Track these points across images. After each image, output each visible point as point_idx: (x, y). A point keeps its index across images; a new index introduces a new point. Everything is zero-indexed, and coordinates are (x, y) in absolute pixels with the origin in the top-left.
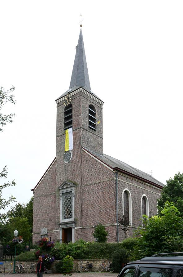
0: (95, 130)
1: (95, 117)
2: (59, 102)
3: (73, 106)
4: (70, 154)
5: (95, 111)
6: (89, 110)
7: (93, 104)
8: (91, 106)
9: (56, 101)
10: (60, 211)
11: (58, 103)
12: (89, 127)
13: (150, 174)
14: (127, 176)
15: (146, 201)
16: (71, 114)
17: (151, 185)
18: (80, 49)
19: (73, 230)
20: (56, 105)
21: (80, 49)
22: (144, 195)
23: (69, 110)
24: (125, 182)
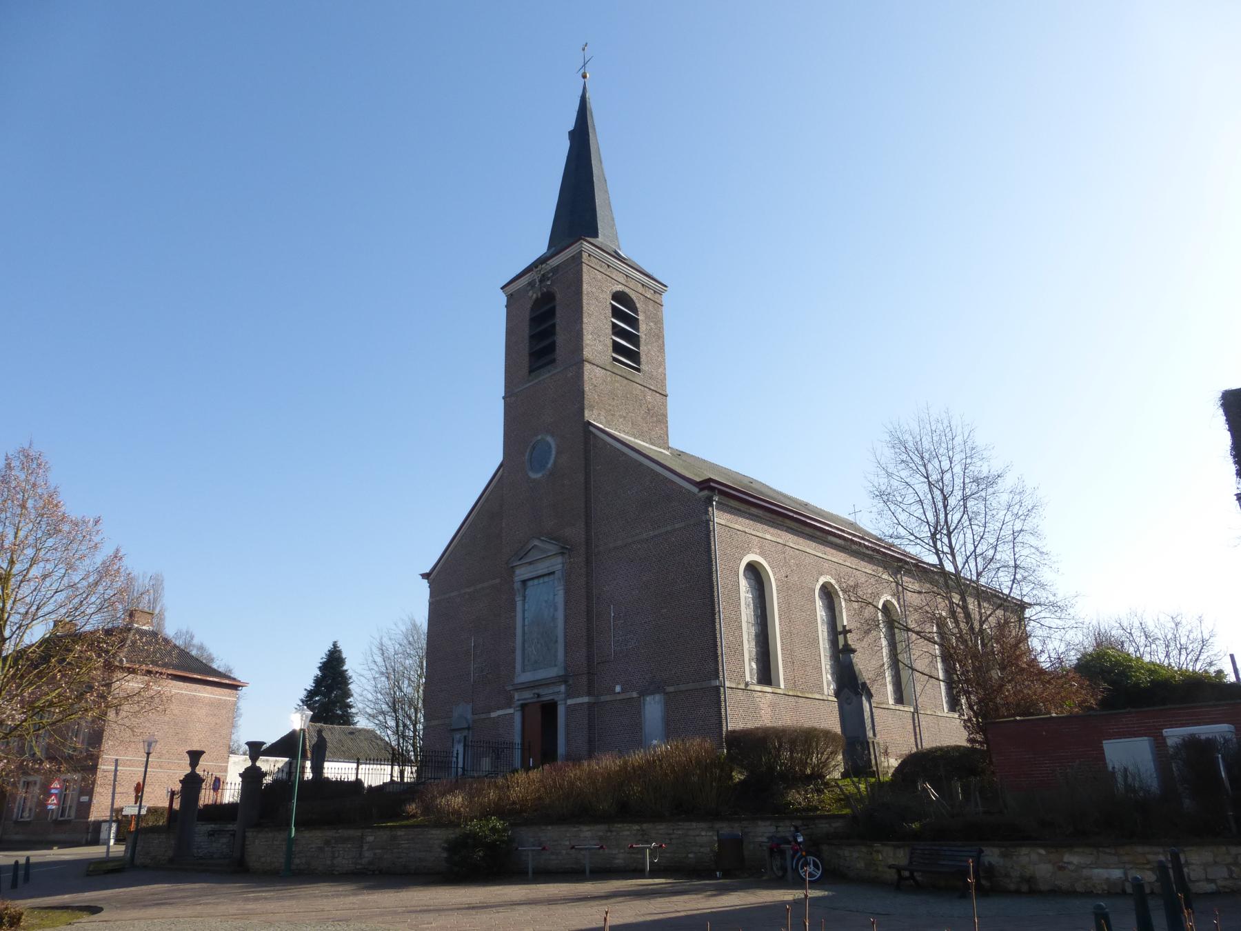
0: (638, 370)
1: (637, 330)
2: (514, 293)
3: (558, 296)
4: (550, 447)
5: (635, 310)
6: (614, 307)
7: (627, 290)
8: (619, 297)
9: (502, 288)
10: (514, 642)
11: (511, 295)
12: (615, 359)
13: (851, 518)
14: (754, 510)
15: (836, 601)
16: (552, 322)
17: (824, 535)
18: (581, 137)
19: (561, 710)
20: (503, 299)
21: (581, 137)
22: (822, 580)
23: (782, 642)
24: (747, 530)
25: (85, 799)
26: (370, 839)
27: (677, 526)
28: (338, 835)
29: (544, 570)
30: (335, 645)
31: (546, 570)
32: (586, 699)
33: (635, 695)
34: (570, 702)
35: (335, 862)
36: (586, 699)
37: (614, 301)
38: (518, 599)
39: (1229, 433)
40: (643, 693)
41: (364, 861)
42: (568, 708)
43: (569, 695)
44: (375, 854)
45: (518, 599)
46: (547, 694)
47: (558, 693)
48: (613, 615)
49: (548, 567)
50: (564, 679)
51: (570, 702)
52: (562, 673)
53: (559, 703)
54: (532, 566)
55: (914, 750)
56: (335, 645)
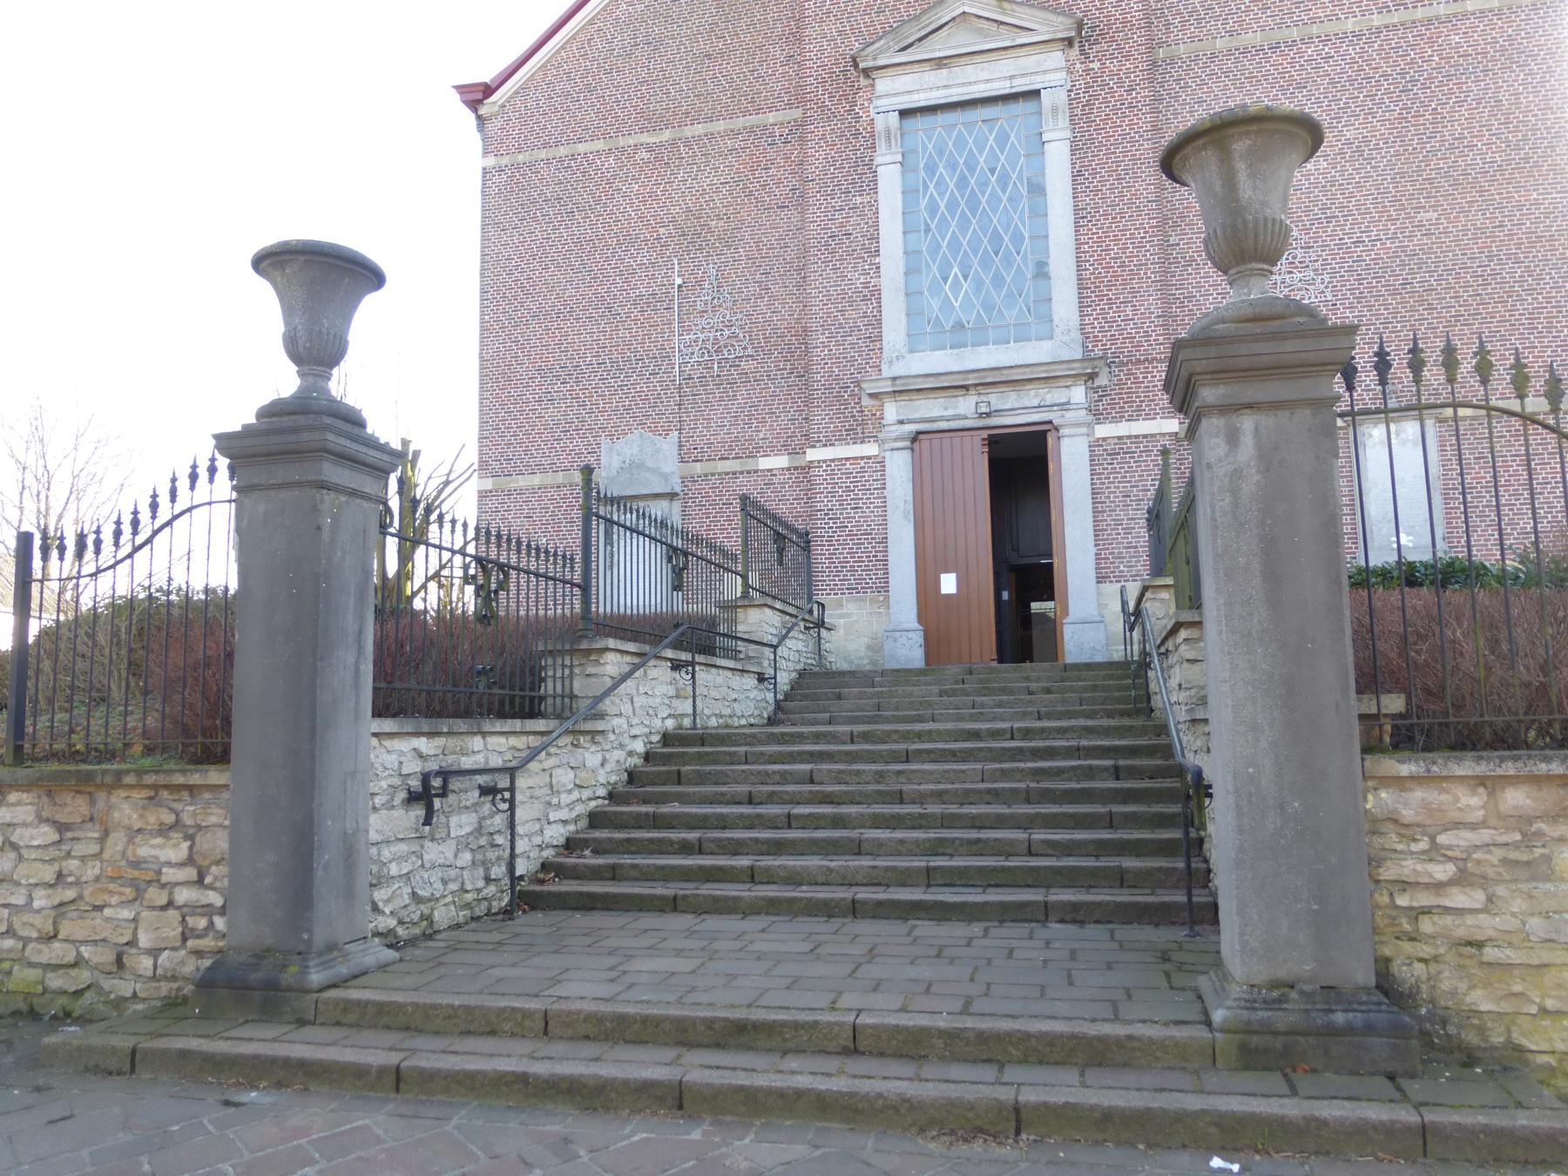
25: (1420, 740)
29: (996, 85)
30: (457, 88)
31: (1007, 83)
32: (813, 455)
34: (1102, 431)
36: (813, 455)
38: (889, 159)
39: (238, 428)
42: (1096, 445)
43: (1098, 416)
45: (889, 159)
47: (1065, 406)
49: (1012, 77)
51: (1102, 431)
54: (944, 71)
56: (457, 88)
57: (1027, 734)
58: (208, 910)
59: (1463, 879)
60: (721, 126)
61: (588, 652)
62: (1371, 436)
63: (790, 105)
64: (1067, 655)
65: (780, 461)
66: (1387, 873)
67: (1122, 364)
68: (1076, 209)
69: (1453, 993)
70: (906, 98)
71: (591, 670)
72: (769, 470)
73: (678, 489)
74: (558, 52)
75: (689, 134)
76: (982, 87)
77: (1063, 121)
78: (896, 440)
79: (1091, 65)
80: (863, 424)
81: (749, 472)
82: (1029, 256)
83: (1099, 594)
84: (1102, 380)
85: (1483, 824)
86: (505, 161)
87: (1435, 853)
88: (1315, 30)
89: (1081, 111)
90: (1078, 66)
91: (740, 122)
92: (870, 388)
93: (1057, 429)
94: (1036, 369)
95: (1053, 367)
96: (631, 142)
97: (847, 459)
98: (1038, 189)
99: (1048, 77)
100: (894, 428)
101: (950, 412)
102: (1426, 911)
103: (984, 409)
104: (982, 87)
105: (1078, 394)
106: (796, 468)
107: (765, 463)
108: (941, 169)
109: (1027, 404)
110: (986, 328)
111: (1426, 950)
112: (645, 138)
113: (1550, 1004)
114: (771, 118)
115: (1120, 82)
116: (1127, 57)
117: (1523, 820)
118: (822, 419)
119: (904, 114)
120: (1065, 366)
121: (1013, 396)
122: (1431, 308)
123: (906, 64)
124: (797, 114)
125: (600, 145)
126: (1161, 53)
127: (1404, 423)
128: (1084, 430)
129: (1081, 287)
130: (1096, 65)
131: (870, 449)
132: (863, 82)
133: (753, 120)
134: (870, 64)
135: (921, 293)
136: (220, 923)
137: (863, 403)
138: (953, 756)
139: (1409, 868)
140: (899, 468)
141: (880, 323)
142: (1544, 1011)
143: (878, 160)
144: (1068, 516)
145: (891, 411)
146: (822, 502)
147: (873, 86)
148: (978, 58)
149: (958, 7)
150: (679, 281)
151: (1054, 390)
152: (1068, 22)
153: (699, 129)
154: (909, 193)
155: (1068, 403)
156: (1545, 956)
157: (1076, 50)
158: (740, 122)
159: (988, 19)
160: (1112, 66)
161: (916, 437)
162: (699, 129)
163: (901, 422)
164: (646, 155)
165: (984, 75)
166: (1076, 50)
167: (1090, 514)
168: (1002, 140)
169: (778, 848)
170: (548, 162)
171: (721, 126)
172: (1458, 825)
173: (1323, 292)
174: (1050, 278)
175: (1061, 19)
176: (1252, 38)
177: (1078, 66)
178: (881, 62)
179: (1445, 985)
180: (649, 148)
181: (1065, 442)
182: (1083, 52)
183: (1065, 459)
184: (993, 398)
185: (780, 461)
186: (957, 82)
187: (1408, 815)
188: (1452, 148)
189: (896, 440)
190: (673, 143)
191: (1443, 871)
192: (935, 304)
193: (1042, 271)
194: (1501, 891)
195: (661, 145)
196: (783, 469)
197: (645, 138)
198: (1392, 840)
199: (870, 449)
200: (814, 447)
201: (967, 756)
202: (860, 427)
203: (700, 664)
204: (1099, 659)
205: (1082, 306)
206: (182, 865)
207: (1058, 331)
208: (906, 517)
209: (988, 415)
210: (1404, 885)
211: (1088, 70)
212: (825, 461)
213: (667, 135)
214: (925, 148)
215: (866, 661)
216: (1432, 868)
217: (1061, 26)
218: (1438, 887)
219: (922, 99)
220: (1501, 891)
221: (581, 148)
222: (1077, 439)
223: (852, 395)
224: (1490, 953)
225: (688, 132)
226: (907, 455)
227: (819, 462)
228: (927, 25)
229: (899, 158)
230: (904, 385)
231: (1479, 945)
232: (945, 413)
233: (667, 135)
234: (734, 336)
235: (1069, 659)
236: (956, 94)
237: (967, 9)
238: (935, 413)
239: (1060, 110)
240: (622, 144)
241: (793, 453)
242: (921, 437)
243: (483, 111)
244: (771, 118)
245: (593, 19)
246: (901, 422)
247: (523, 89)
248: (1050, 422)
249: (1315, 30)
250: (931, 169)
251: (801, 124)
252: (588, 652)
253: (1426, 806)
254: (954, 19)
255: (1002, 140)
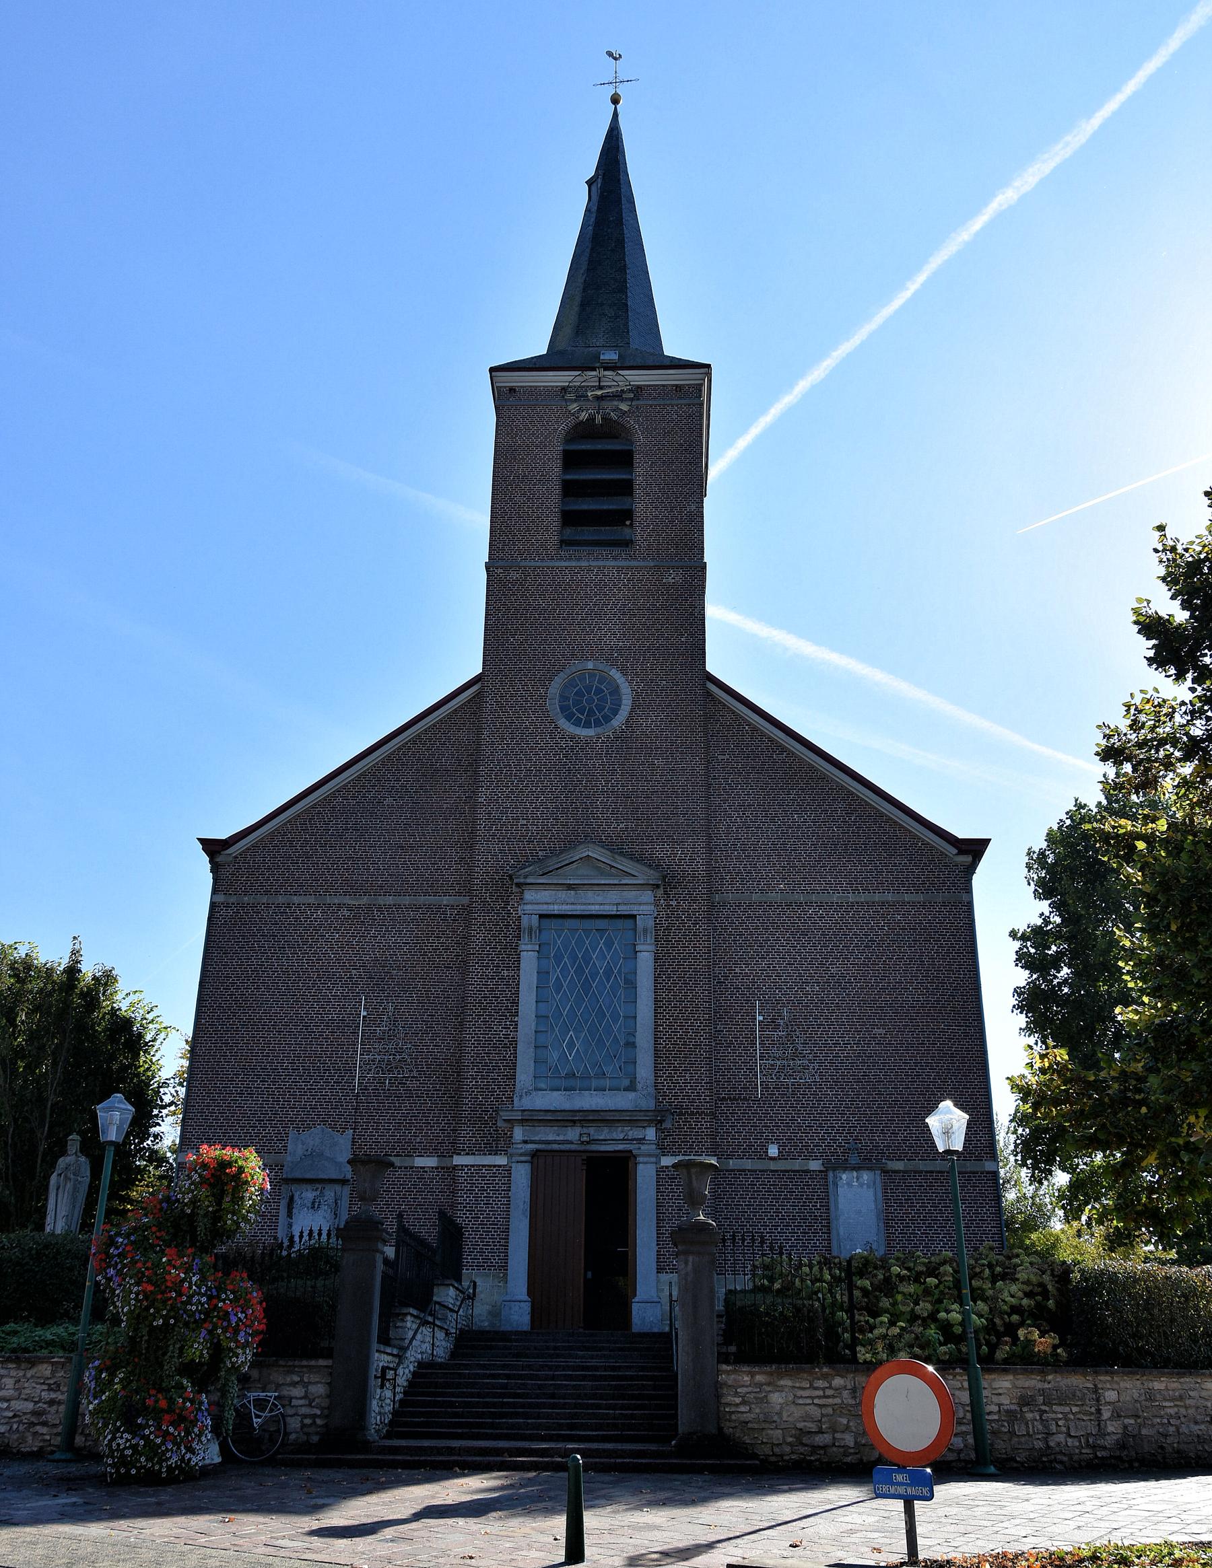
26: (1111, 1396)
27: (907, 898)
28: (1046, 1386)
29: (607, 908)
30: (202, 841)
32: (458, 1160)
33: (815, 1165)
35: (1052, 1444)
36: (458, 1160)
37: (623, 480)
38: (529, 947)
40: (836, 1165)
41: (1109, 1441)
42: (661, 1170)
43: (663, 1150)
44: (1125, 1427)
46: (610, 1140)
47: (641, 1141)
48: (363, 1013)
49: (617, 904)
50: (657, 1118)
52: (651, 1104)
53: (640, 1159)
55: (435, 1298)
56: (202, 841)
57: (613, 1369)
58: (314, 1416)
59: (744, 1403)
60: (407, 900)
61: (398, 1315)
62: (841, 1179)
63: (460, 894)
64: (634, 1326)
65: (430, 1162)
66: (723, 1401)
67: (681, 1114)
68: (656, 1000)
69: (739, 1437)
70: (545, 907)
71: (399, 1324)
72: (421, 1168)
73: (349, 1176)
74: (285, 824)
75: (382, 903)
76: (597, 907)
77: (650, 939)
78: (521, 1155)
79: (671, 903)
80: (497, 1140)
81: (406, 1168)
82: (623, 1030)
83: (658, 1281)
84: (667, 1125)
85: (750, 1386)
86: (233, 899)
87: (736, 1394)
88: (814, 898)
89: (662, 936)
90: (662, 901)
91: (422, 899)
92: (505, 1115)
93: (635, 1157)
94: (624, 1113)
95: (634, 1113)
96: (336, 901)
97: (483, 1166)
98: (631, 984)
99: (642, 907)
100: (520, 1146)
101: (561, 1138)
102: (733, 1412)
103: (585, 1138)
104: (597, 907)
105: (651, 1133)
106: (443, 1168)
107: (420, 1162)
108: (566, 959)
109: (615, 1137)
110: (590, 1078)
111: (733, 1425)
112: (348, 900)
113: (764, 1440)
114: (445, 900)
115: (689, 917)
116: (695, 901)
117: (760, 1385)
118: (466, 1134)
119: (542, 916)
120: (642, 1114)
121: (606, 1130)
122: (880, 1094)
123: (547, 884)
124: (465, 900)
125: (311, 900)
126: (717, 898)
127: (862, 1172)
128: (653, 1159)
129: (656, 1056)
130: (674, 903)
131: (501, 1160)
132: (515, 889)
133: (431, 899)
134: (522, 880)
135: (547, 1047)
136: (319, 1422)
137: (499, 1124)
138: (577, 1378)
139: (729, 1399)
140: (521, 1176)
141: (515, 1065)
142: (763, 1443)
143: (523, 947)
144: (640, 1198)
145: (518, 1133)
146: (463, 1198)
147: (522, 893)
148: (596, 888)
149: (585, 852)
150: (363, 1013)
151: (634, 1129)
152: (657, 875)
153: (390, 900)
154: (542, 974)
155: (644, 1139)
156: (764, 1425)
157: (660, 892)
158: (422, 899)
159: (604, 862)
160: (685, 906)
161: (535, 1154)
162: (390, 900)
163: (525, 1142)
164: (346, 913)
165: (599, 899)
166: (660, 892)
167: (655, 1222)
168: (609, 945)
169: (502, 1415)
170: (268, 906)
171: (407, 900)
172: (743, 1386)
173: (814, 1075)
174: (636, 1047)
175: (652, 872)
176: (773, 896)
177: (662, 901)
178: (528, 881)
179: (737, 1435)
180: (350, 908)
181: (640, 1167)
182: (665, 893)
183: (639, 1180)
184: (592, 1131)
185: (430, 1162)
186: (580, 901)
187: (730, 1383)
188: (894, 988)
189: (521, 1155)
190: (369, 907)
191: (738, 1400)
192: (555, 1055)
193: (631, 1045)
194: (753, 1406)
195: (359, 907)
196: (433, 1168)
197: (348, 900)
198: (725, 1391)
199: (501, 1160)
200: (460, 1154)
201: (584, 1378)
202: (496, 1142)
203: (438, 1326)
204: (656, 1330)
205: (656, 1069)
206: (301, 1398)
207: (639, 1086)
208: (524, 1214)
209: (588, 1143)
210: (729, 1405)
211: (668, 906)
212: (467, 1166)
213: (365, 900)
214: (555, 942)
215: (486, 1324)
216: (736, 1399)
217: (652, 876)
218: (737, 1405)
219: (556, 909)
220: (753, 1406)
221: (296, 899)
222: (649, 1166)
223: (491, 1117)
224: (750, 1425)
225: (381, 900)
226: (528, 1167)
227: (462, 1166)
228: (563, 860)
229: (537, 948)
230: (530, 1115)
231: (747, 1423)
232: (558, 1138)
233: (365, 900)
234: (403, 1060)
235: (635, 1329)
236: (579, 909)
237: (590, 854)
238: (551, 1137)
239: (649, 932)
240: (328, 902)
241: (441, 1156)
242: (539, 1154)
243: (219, 859)
244: (445, 900)
245: (315, 804)
246: (525, 1142)
247: (254, 846)
248: (631, 1151)
249: (814, 898)
250: (559, 958)
251: (467, 910)
252: (398, 1315)
253: (735, 1380)
254: (581, 859)
255: (609, 945)
